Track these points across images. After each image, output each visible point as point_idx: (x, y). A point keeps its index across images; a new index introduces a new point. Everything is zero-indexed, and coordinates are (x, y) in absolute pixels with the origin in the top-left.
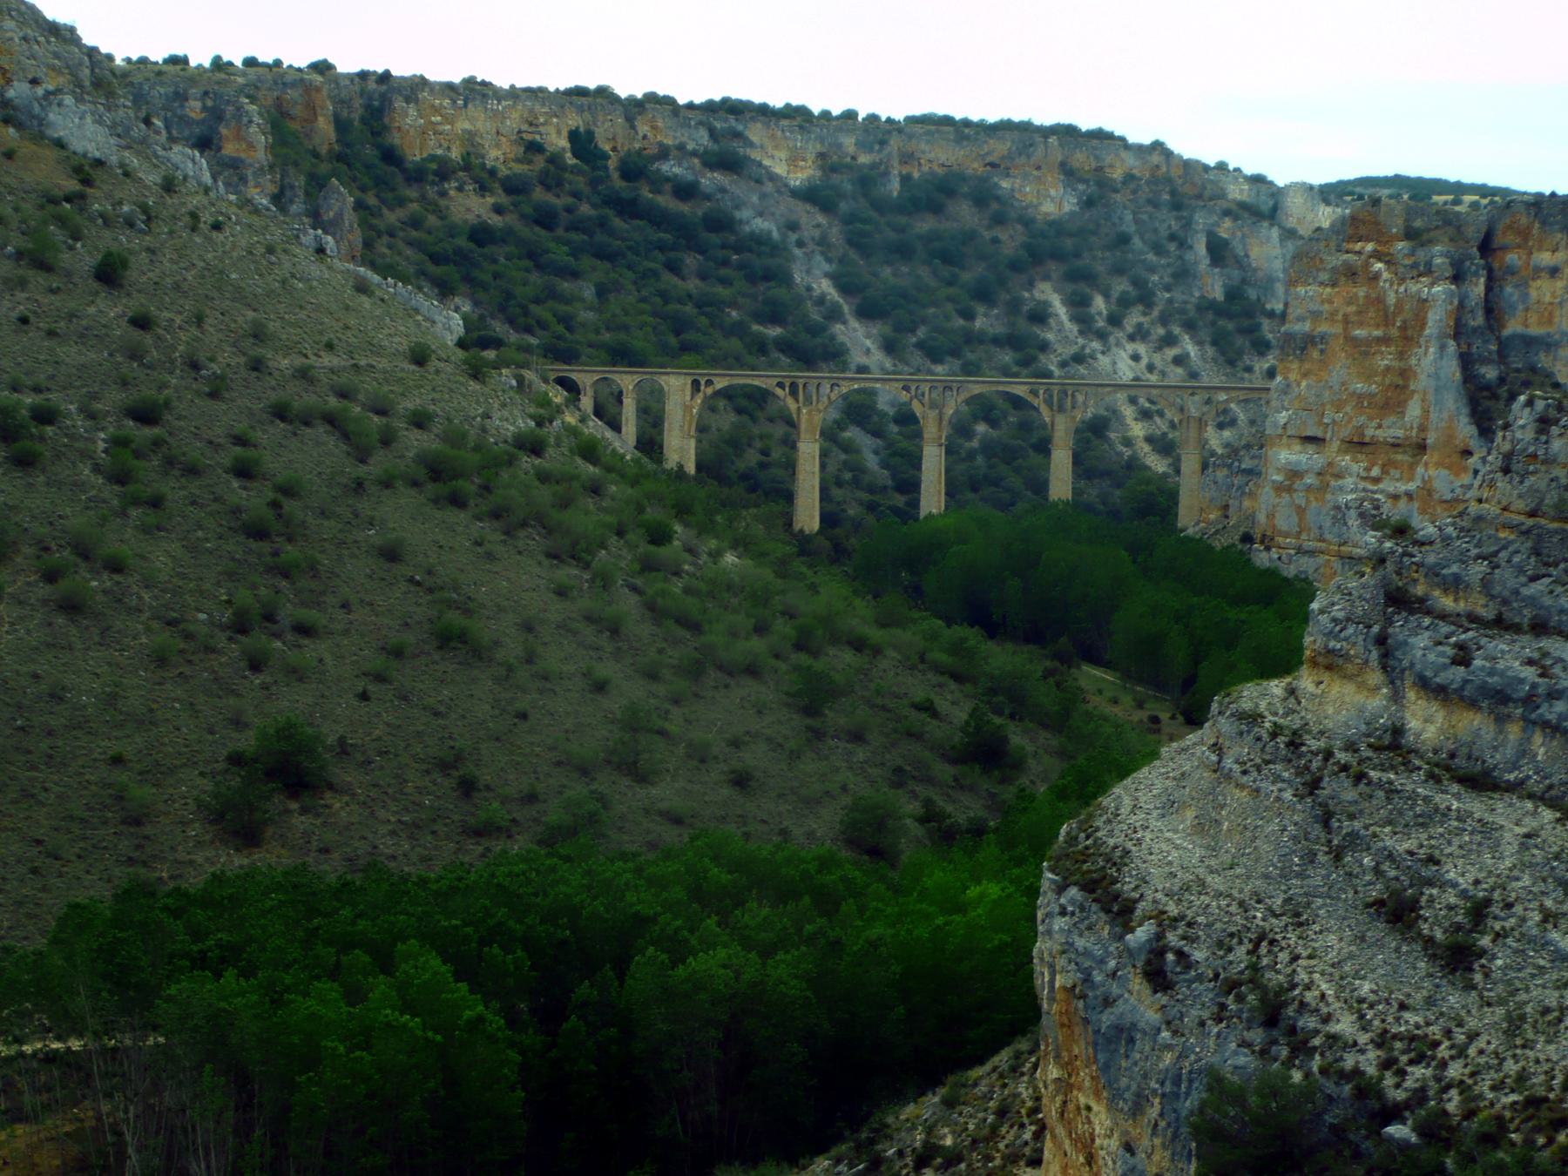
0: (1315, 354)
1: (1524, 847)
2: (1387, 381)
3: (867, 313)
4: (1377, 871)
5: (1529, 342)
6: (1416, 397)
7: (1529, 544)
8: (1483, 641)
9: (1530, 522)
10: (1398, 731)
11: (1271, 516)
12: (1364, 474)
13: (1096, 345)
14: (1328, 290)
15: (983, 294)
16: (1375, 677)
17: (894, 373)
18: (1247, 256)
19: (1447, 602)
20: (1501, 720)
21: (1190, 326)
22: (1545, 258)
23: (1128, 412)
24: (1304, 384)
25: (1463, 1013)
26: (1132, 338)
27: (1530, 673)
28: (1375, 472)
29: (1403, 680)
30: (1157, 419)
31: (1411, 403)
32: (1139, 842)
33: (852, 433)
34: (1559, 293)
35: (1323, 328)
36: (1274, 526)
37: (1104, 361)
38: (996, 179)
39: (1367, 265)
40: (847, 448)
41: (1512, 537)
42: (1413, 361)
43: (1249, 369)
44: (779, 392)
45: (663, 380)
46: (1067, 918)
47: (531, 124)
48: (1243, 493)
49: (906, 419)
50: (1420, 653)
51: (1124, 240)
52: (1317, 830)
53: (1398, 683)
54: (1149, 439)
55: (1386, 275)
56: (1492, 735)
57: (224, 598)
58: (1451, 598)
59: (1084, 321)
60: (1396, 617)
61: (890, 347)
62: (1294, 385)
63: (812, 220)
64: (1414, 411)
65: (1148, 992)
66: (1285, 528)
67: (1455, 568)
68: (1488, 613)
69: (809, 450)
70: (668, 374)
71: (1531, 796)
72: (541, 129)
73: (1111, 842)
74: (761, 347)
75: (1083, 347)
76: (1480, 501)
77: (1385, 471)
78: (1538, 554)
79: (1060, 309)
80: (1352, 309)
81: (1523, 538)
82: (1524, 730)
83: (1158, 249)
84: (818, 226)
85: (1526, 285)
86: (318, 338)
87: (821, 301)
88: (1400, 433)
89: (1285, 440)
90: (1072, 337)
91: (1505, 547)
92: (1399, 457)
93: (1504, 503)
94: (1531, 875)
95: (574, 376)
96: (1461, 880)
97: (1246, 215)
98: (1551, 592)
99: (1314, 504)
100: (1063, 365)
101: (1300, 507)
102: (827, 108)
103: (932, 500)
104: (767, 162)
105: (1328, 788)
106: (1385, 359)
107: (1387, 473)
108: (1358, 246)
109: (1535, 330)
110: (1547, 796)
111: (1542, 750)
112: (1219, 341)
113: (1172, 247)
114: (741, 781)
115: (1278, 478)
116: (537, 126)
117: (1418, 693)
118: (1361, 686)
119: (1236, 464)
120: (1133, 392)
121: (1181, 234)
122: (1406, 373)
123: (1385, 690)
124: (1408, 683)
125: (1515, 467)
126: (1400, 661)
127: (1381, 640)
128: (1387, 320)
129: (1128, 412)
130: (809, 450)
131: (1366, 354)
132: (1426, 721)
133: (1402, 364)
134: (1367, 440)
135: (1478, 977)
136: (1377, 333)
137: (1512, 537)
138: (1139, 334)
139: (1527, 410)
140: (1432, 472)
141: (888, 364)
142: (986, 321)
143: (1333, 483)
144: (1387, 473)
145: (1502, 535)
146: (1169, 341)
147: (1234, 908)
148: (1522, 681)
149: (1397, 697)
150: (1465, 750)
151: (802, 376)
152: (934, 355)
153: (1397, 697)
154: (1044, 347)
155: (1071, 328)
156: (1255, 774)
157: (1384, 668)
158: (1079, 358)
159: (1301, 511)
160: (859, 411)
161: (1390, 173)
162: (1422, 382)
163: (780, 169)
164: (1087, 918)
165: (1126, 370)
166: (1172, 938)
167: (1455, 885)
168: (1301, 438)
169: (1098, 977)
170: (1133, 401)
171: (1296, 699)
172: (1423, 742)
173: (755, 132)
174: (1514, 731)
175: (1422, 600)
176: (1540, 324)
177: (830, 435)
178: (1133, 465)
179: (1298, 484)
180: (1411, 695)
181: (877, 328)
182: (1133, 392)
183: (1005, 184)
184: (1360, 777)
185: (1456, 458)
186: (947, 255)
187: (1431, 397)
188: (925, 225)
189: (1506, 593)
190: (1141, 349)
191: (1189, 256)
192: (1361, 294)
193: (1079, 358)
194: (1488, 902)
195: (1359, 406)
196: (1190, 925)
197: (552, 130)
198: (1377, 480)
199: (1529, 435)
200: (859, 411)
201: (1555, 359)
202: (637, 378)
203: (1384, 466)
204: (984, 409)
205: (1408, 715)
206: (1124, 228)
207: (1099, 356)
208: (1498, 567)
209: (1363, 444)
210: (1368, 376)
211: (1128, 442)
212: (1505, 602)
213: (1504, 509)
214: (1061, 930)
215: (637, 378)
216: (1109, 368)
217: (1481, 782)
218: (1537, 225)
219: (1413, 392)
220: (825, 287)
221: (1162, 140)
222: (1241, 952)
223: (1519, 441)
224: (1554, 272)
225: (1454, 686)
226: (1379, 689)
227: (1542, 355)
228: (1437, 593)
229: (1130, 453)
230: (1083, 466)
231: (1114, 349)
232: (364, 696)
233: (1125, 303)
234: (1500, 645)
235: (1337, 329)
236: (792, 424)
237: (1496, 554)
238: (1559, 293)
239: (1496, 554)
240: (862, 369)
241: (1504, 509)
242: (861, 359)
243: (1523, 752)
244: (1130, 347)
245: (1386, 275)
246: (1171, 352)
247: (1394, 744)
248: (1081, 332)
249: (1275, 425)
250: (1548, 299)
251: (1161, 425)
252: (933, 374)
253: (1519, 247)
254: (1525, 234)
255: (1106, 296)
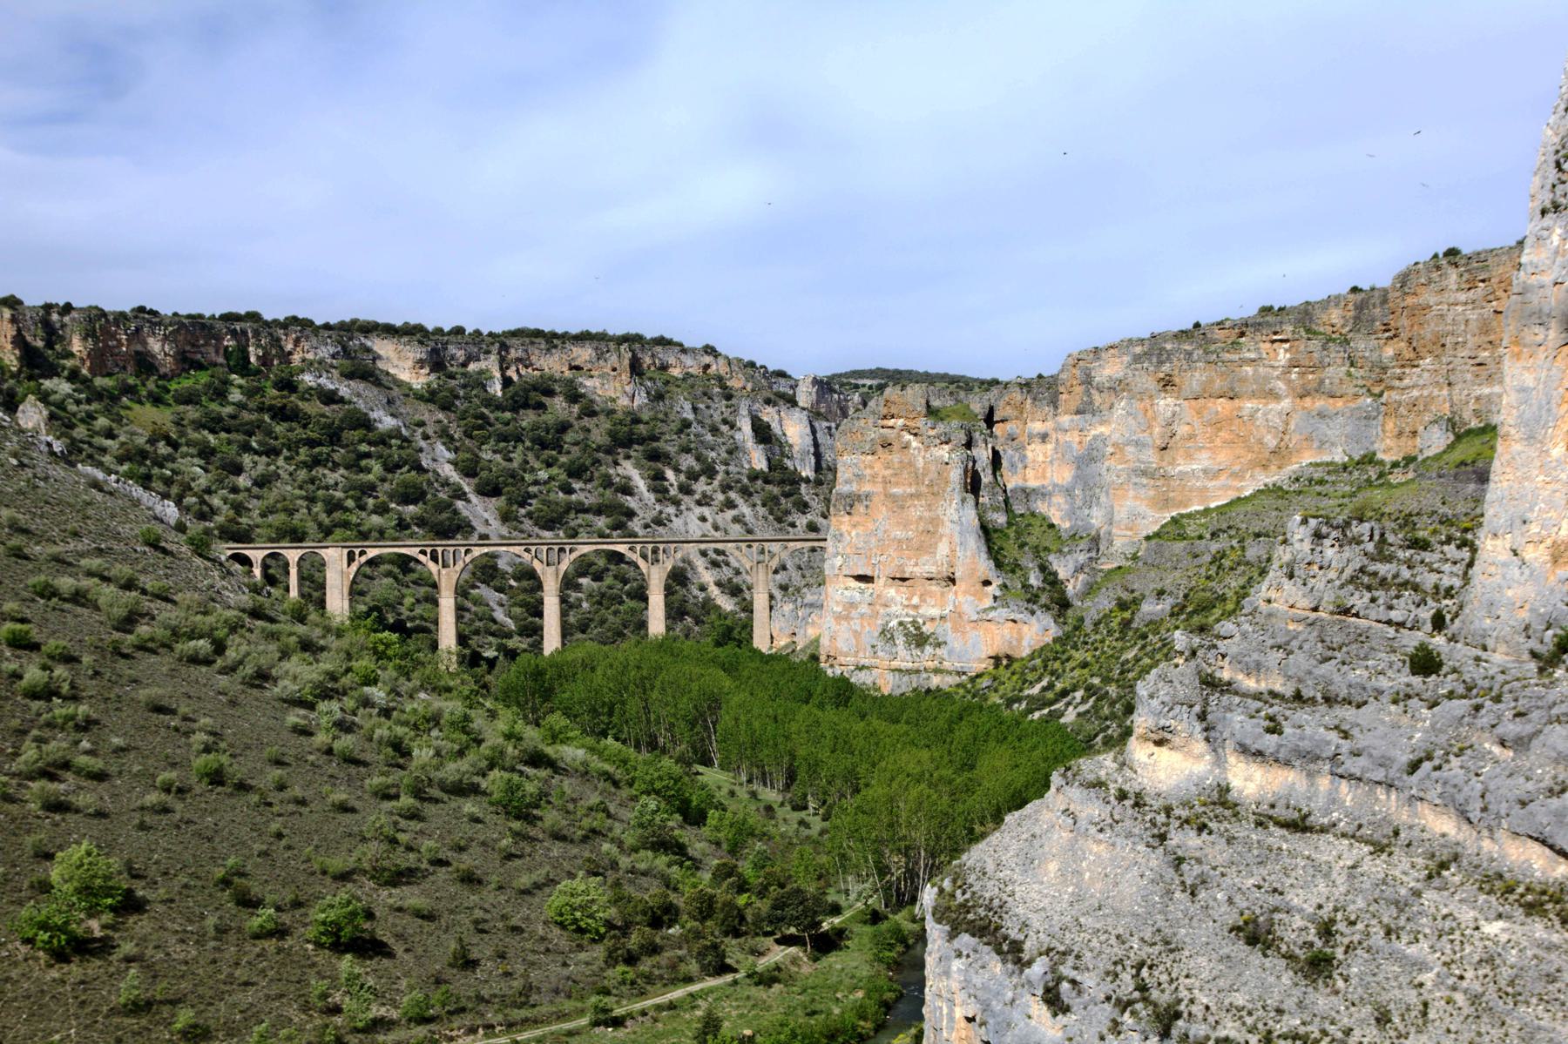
0: (862, 509)
1: (1351, 877)
2: (921, 528)
3: (489, 490)
4: (1230, 901)
5: (1027, 493)
6: (944, 539)
7: (1315, 634)
8: (1288, 713)
9: (1313, 615)
10: (1224, 790)
11: (833, 638)
12: (906, 603)
13: (671, 510)
14: (869, 457)
15: (576, 472)
16: (1200, 746)
17: (510, 538)
18: (784, 435)
19: (1250, 684)
20: (1311, 775)
21: (746, 493)
22: (1037, 427)
23: (700, 563)
24: (853, 533)
25: (1333, 1013)
26: (699, 503)
27: (1333, 736)
28: (915, 600)
29: (1224, 748)
30: (725, 568)
31: (940, 545)
32: (1012, 894)
33: (485, 592)
34: (1049, 453)
35: (867, 488)
36: (836, 649)
37: (677, 523)
38: (580, 380)
39: (899, 437)
40: (478, 602)
41: (1301, 628)
42: (940, 512)
43: (793, 525)
44: (422, 558)
45: (322, 552)
46: (964, 959)
47: (193, 345)
48: (807, 623)
49: (529, 575)
50: (1239, 725)
51: (686, 424)
52: (1170, 873)
53: (1220, 750)
54: (719, 584)
55: (914, 444)
56: (1305, 787)
57: (10, 750)
58: (1253, 680)
59: (660, 490)
60: (1212, 698)
61: (506, 517)
62: (846, 534)
63: (432, 416)
64: (943, 549)
65: (1048, 1015)
66: (845, 649)
67: (1255, 656)
68: (1288, 691)
69: (447, 603)
70: (327, 547)
71: (1344, 835)
72: (202, 349)
73: (987, 895)
74: (402, 525)
75: (661, 512)
76: (1269, 601)
77: (923, 600)
78: (1323, 641)
79: (640, 484)
80: (888, 472)
81: (1309, 629)
82: (1332, 782)
83: (715, 430)
84: (439, 422)
85: (1024, 448)
86: (63, 527)
87: (446, 483)
88: (933, 569)
89: (841, 578)
90: (650, 504)
91: (1295, 638)
92: (934, 588)
93: (1291, 602)
94: (1364, 898)
95: (247, 552)
96: (1305, 906)
97: (781, 403)
98: (1339, 670)
99: (867, 629)
100: (646, 526)
101: (856, 631)
102: (439, 325)
103: (552, 640)
104: (392, 371)
105: (1175, 838)
106: (917, 510)
107: (925, 601)
108: (891, 422)
109: (1032, 483)
110: (1358, 834)
111: (1349, 798)
112: (771, 502)
113: (724, 428)
114: (470, 880)
115: (838, 609)
116: (198, 347)
117: (1238, 757)
118: (1189, 754)
119: (799, 600)
120: (703, 546)
121: (731, 418)
122: (936, 522)
123: (1208, 757)
124: (1228, 751)
125: (1296, 573)
126: (1221, 733)
127: (1202, 717)
128: (917, 478)
129: (700, 563)
130: (447, 603)
131: (902, 507)
132: (1246, 780)
133: (932, 514)
134: (907, 576)
135: (1340, 984)
136: (912, 490)
137: (1301, 628)
138: (704, 501)
139: (1302, 528)
140: (961, 598)
141: (504, 531)
142: (584, 493)
143: (882, 611)
144: (925, 601)
145: (1291, 627)
146: (730, 505)
147: (1113, 941)
148: (1328, 743)
149: (1219, 762)
150: (1283, 802)
151: (441, 545)
152: (549, 524)
153: (1219, 762)
154: (631, 514)
155: (650, 497)
156: (1109, 831)
157: (1207, 740)
158: (659, 522)
159: (856, 634)
160: (487, 571)
161: (874, 367)
162: (947, 529)
163: (405, 376)
164: (980, 958)
165: (696, 529)
166: (1066, 970)
167: (1300, 911)
168: (854, 577)
169: (997, 1006)
170: (704, 554)
171: (1131, 769)
172: (1247, 797)
173: (383, 347)
174: (1324, 783)
175: (1229, 684)
176: (1036, 478)
177: (462, 592)
178: (708, 606)
179: (854, 613)
180: (1232, 759)
181: (494, 502)
182: (703, 546)
183: (588, 383)
184: (1202, 828)
185: (979, 586)
186: (549, 441)
187: (957, 539)
188: (528, 418)
189: (1301, 674)
190: (706, 511)
191: (738, 436)
192: (896, 460)
193: (659, 522)
194: (1333, 921)
195: (899, 549)
196: (1078, 957)
197: (211, 350)
198: (916, 607)
199: (1307, 546)
200: (487, 571)
201: (1049, 505)
202: (300, 552)
203: (922, 595)
204: (584, 567)
205: (1230, 776)
206: (685, 415)
207: (673, 518)
208: (1291, 652)
209: (904, 580)
210: (905, 525)
211: (703, 588)
212: (1300, 681)
213: (1292, 607)
214: (959, 970)
215: (300, 552)
216: (683, 529)
217: (1299, 825)
218: (1029, 401)
219: (941, 536)
220: (448, 471)
221: (711, 344)
222: (1127, 977)
223: (1298, 552)
224: (1044, 437)
225: (1271, 750)
226: (1203, 756)
227: (1039, 503)
228: (1240, 677)
229: (703, 595)
230: (675, 612)
231: (685, 513)
232: (142, 827)
233: (693, 476)
234: (1303, 715)
235: (878, 488)
236: (435, 586)
237: (1288, 643)
238: (1049, 453)
239: (1288, 643)
240: (484, 537)
241: (1292, 607)
242: (481, 529)
243: (1333, 800)
244: (698, 510)
245: (914, 444)
246: (730, 514)
247: (1223, 799)
248: (659, 501)
249: (833, 567)
250: (1041, 458)
251: (727, 573)
252: (541, 538)
253: (1017, 418)
254: (1020, 408)
255: (677, 470)
